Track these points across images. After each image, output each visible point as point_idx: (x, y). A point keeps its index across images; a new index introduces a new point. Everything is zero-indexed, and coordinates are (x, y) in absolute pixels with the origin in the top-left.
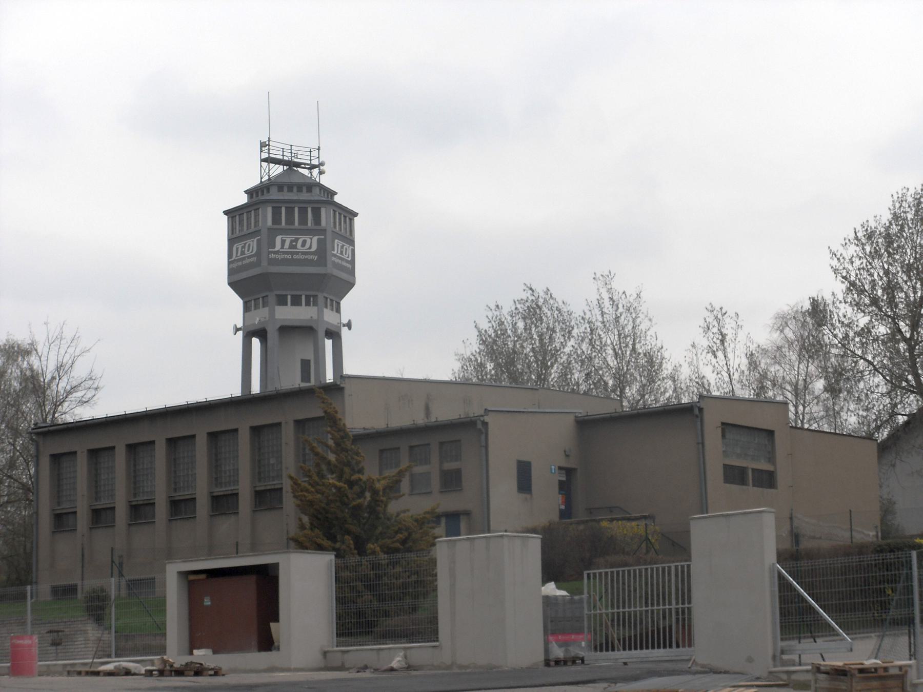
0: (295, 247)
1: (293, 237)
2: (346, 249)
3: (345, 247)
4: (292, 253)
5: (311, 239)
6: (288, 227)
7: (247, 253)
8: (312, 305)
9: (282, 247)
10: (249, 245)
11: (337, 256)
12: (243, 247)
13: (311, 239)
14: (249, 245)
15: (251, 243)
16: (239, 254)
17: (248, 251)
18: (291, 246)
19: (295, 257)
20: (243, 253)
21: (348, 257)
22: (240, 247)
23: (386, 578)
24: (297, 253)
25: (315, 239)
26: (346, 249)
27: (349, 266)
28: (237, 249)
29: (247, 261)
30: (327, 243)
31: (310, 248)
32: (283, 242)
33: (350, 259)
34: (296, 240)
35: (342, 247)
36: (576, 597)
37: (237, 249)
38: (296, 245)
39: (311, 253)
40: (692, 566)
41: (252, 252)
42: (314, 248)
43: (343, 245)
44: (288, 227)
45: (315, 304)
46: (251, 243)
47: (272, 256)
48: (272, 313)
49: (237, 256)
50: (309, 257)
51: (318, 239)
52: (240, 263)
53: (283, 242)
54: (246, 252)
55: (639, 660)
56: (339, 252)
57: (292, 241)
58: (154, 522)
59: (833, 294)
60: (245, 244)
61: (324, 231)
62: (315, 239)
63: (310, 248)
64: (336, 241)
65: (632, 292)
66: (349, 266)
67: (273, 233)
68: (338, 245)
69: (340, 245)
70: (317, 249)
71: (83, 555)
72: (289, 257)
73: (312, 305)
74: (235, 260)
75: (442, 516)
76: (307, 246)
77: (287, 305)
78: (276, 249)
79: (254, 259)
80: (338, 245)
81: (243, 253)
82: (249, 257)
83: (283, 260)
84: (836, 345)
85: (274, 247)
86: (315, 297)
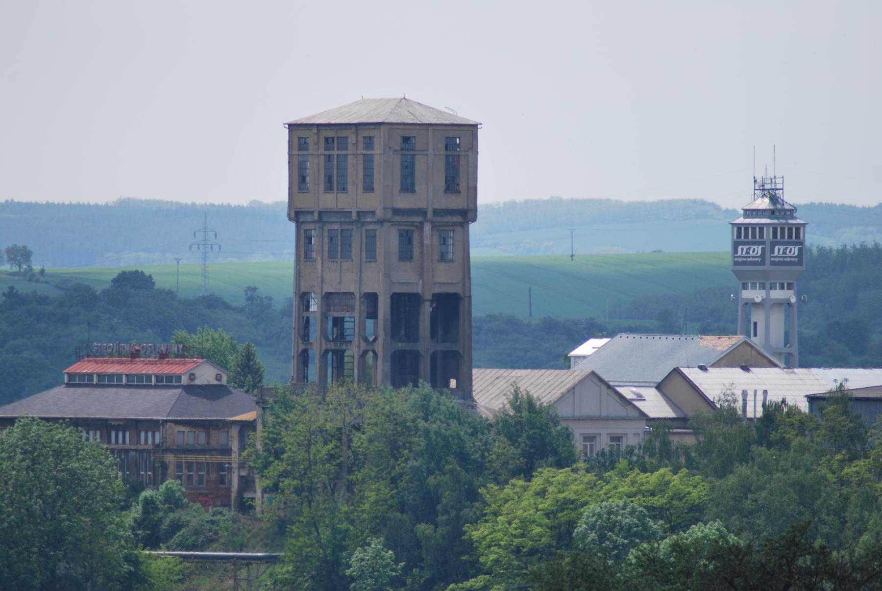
1: (747, 247)
6: (797, 240)
8: (758, 289)
19: (749, 259)
30: (766, 250)
31: (794, 254)
39: (757, 257)
40: (437, 207)
42: (759, 254)
44: (797, 240)
45: (764, 288)
47: (773, 259)
48: (768, 294)
50: (793, 259)
55: (441, 224)
57: (784, 249)
58: (331, 189)
61: (764, 243)
63: (794, 254)
65: (873, 243)
67: (773, 245)
70: (798, 255)
71: (357, 195)
73: (758, 289)
75: (321, 155)
76: (792, 252)
78: (775, 255)
83: (791, 262)
84: (387, 513)
85: (737, 253)
86: (764, 284)
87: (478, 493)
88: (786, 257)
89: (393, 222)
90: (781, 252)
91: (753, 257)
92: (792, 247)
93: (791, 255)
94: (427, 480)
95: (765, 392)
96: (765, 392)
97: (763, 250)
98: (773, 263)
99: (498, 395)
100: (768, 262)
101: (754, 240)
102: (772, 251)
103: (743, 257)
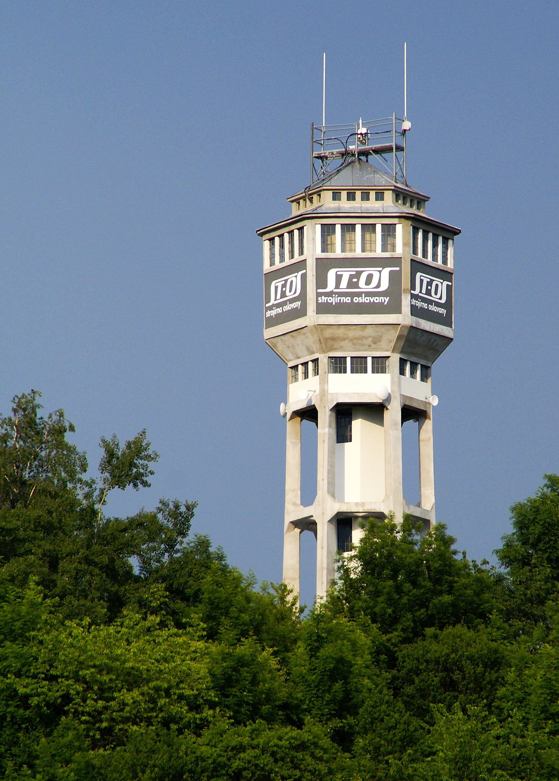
0: (356, 285)
1: (353, 271)
2: (437, 286)
3: (434, 284)
4: (352, 295)
5: (380, 272)
7: (290, 295)
9: (337, 286)
10: (292, 282)
11: (421, 297)
12: (284, 286)
13: (380, 272)
14: (292, 282)
15: (294, 279)
16: (279, 296)
17: (290, 291)
18: (351, 284)
19: (356, 300)
20: (283, 295)
21: (441, 298)
22: (280, 285)
23: (166, 647)
24: (359, 294)
25: (386, 272)
26: (437, 286)
27: (442, 311)
28: (276, 288)
29: (287, 308)
31: (378, 286)
32: (339, 278)
33: (443, 301)
34: (358, 274)
35: (430, 283)
36: (313, 653)
37: (276, 288)
38: (357, 282)
41: (295, 293)
42: (385, 286)
43: (432, 281)
46: (294, 279)
49: (276, 300)
51: (391, 272)
52: (279, 310)
53: (339, 278)
54: (288, 293)
56: (424, 291)
59: (32, 390)
60: (286, 281)
62: (386, 272)
63: (378, 286)
64: (419, 274)
66: (442, 311)
68: (422, 281)
69: (425, 281)
72: (347, 300)
74: (273, 305)
77: (345, 372)
78: (328, 290)
79: (298, 304)
80: (422, 281)
81: (283, 295)
82: (292, 301)
87: (61, 717)
88: (359, 294)
89: (348, 165)
90: (344, 283)
91: (368, 294)
92: (374, 271)
93: (370, 288)
94: (100, 710)
95: (540, 487)
96: (540, 487)
97: (395, 278)
98: (322, 309)
99: (322, 563)
100: (311, 308)
101: (348, 255)
102: (321, 282)
103: (341, 294)
